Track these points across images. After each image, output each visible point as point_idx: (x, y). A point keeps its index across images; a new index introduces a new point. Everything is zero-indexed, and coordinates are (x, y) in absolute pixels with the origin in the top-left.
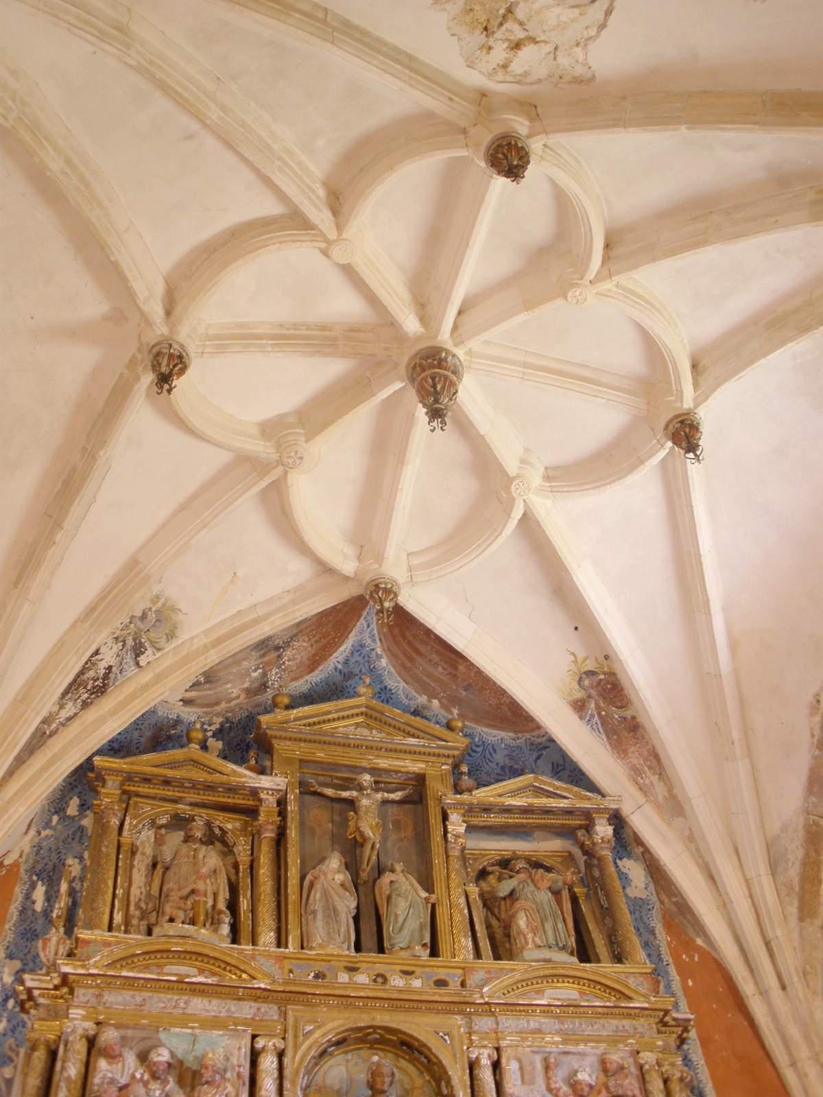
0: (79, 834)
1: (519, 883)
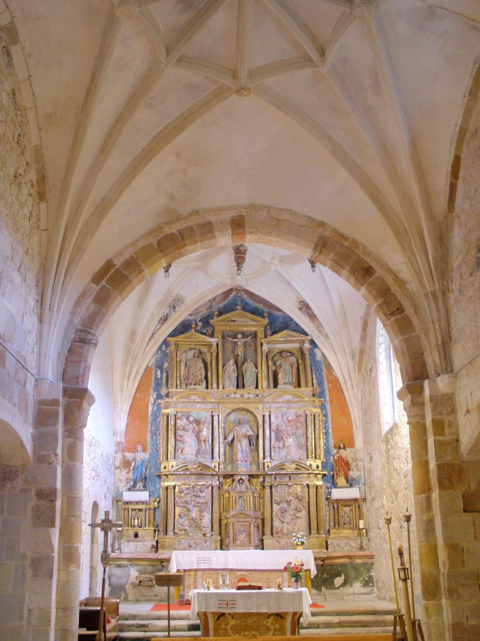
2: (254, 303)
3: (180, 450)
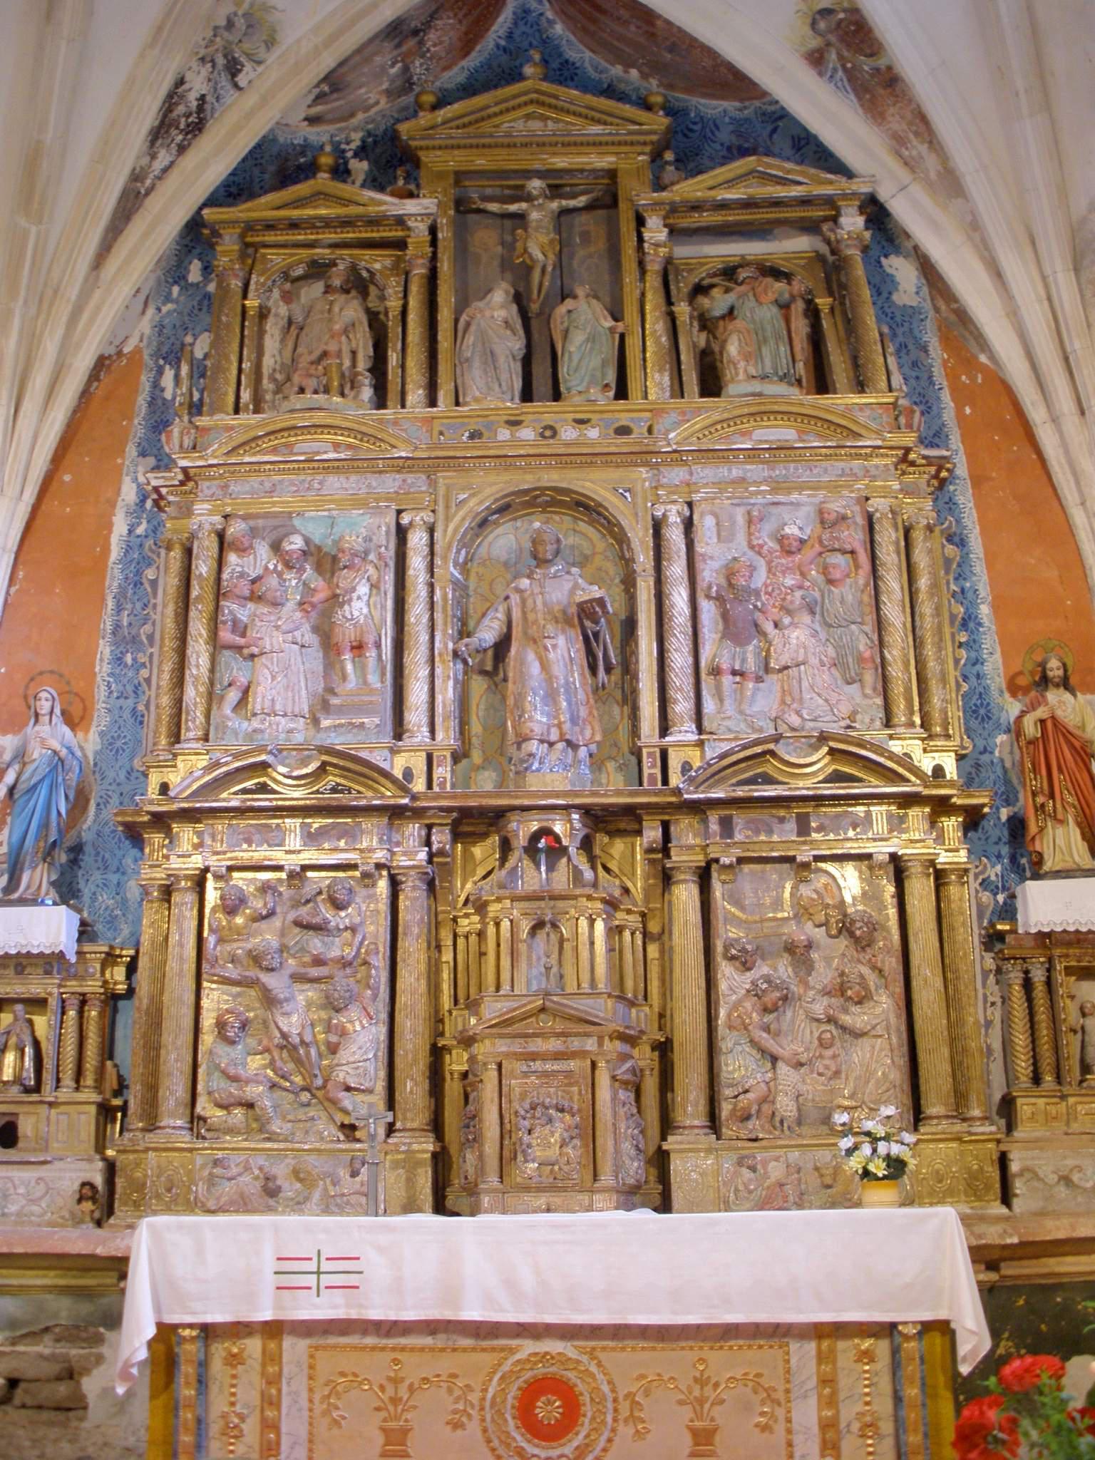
0: (206, 302)
1: (739, 297)
2: (604, 64)
3: (233, 696)
